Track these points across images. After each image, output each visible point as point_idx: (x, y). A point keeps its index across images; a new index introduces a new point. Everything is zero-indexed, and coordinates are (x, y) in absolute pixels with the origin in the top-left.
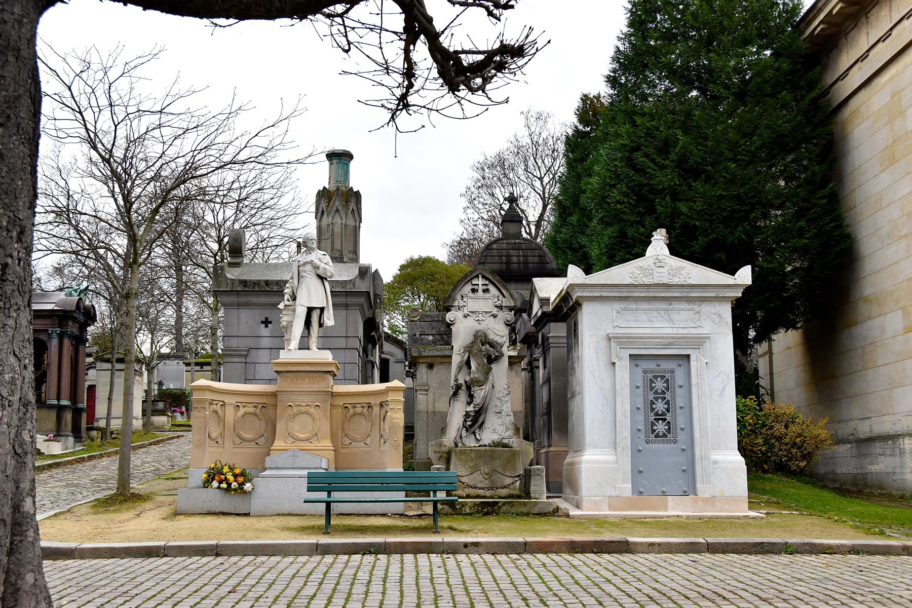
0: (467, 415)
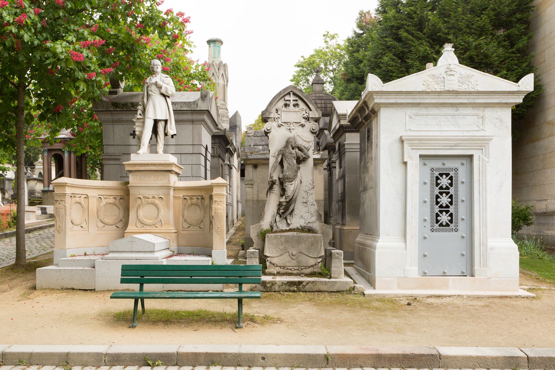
0: (280, 204)
